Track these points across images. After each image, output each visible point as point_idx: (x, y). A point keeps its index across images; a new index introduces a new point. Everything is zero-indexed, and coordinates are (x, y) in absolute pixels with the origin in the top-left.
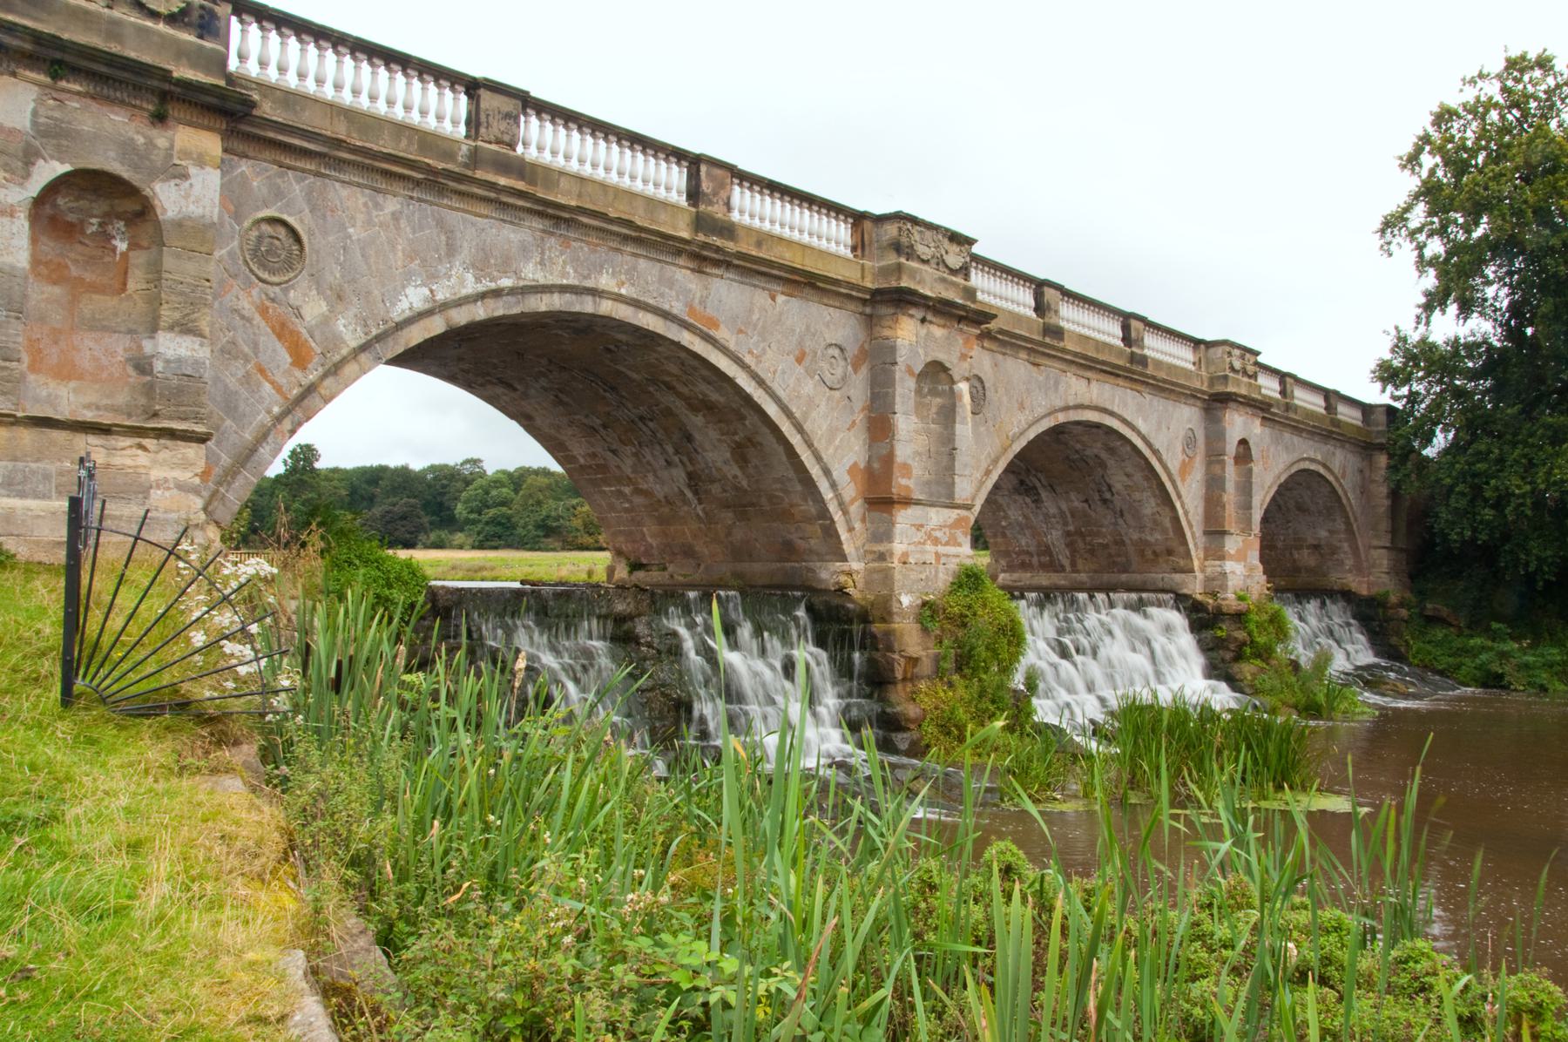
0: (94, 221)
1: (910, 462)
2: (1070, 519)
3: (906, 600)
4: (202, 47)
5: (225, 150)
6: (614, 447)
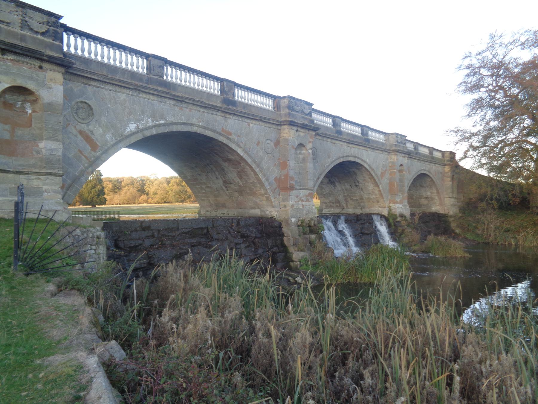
0: (19, 103)
1: (294, 176)
2: (345, 191)
3: (293, 220)
4: (54, 44)
5: (64, 79)
6: (199, 173)
